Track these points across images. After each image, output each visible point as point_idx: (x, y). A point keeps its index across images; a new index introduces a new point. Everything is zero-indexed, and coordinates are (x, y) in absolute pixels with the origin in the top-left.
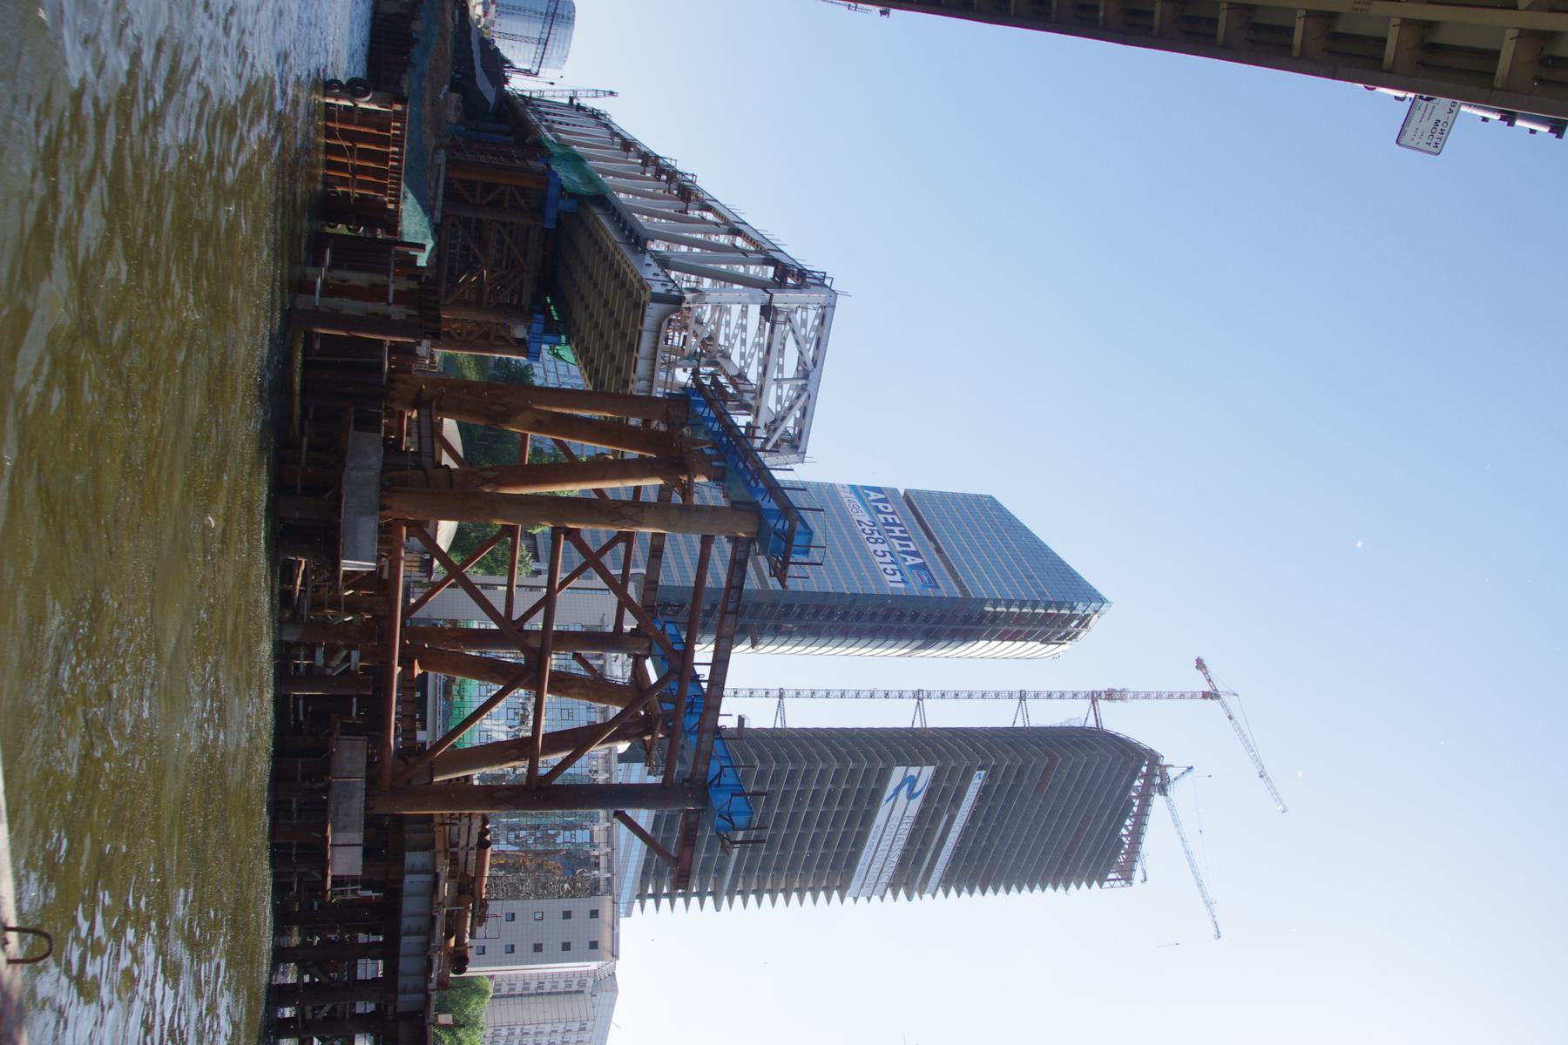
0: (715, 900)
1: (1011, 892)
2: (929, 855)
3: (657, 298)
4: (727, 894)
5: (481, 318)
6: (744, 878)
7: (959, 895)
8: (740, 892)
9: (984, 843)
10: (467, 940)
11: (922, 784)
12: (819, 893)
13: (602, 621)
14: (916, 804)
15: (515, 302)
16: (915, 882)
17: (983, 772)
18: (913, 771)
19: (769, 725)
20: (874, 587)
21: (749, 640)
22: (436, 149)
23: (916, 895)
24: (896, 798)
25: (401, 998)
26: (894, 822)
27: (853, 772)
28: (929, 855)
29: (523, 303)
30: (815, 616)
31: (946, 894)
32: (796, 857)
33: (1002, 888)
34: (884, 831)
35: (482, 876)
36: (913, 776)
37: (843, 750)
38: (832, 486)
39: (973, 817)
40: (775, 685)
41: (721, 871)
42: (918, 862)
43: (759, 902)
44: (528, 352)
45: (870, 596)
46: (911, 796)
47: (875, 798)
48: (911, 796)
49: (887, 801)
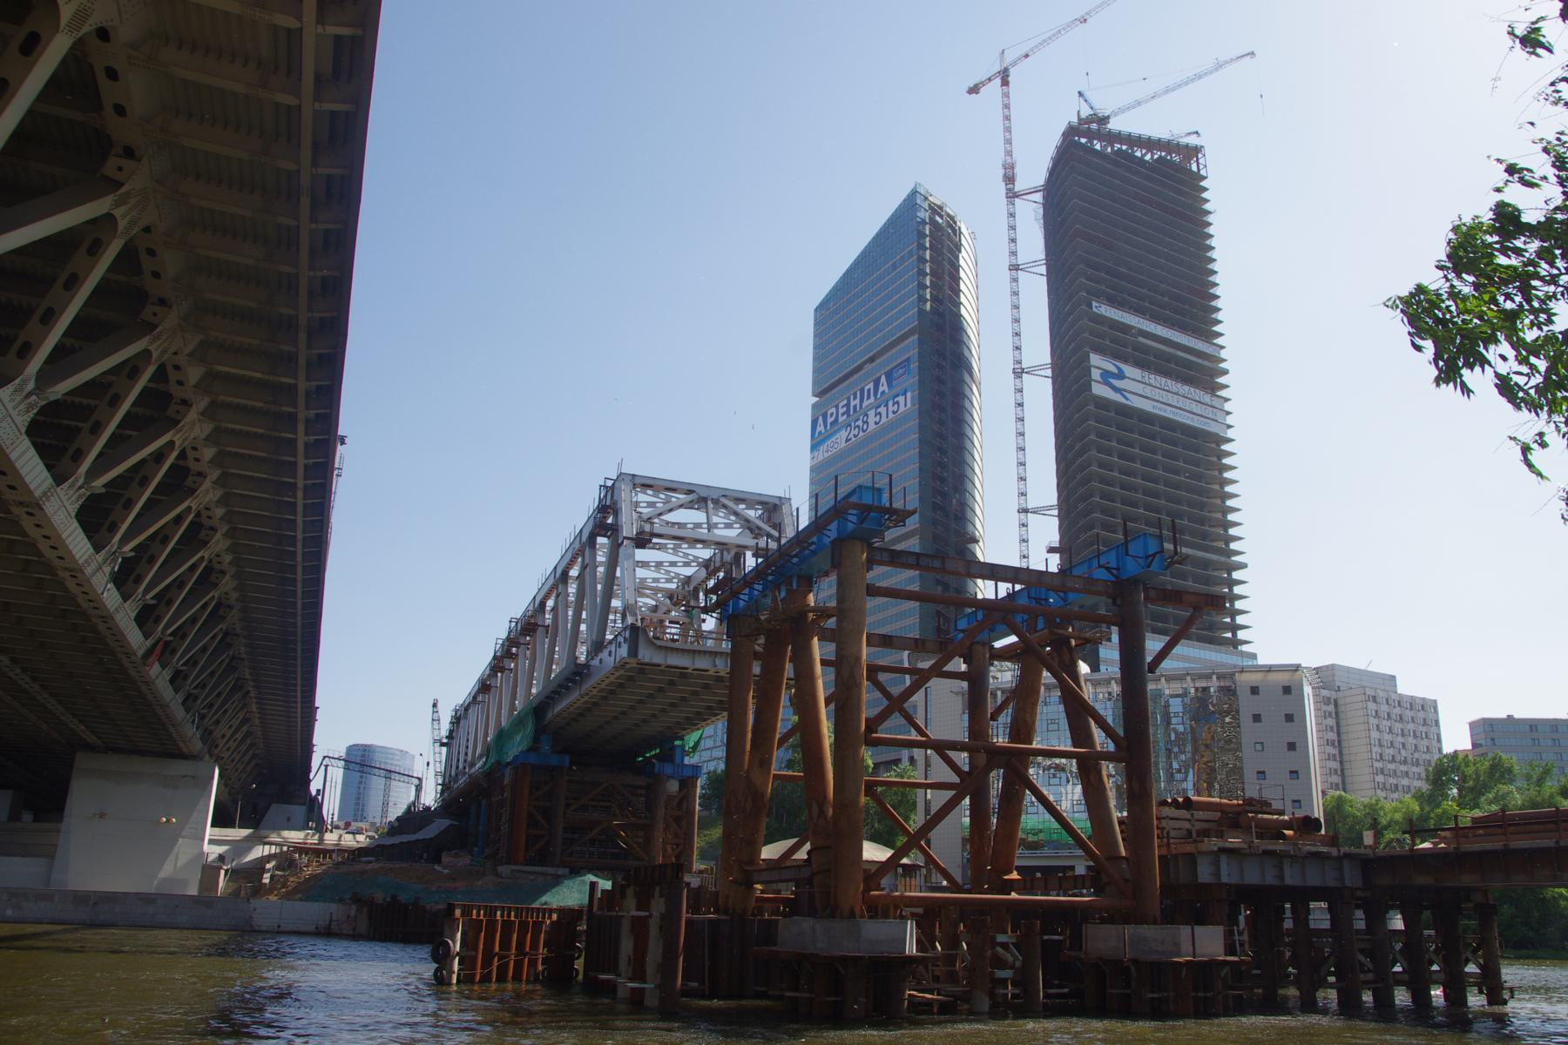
2: (1180, 354)
3: (633, 652)
5: (661, 825)
6: (1213, 541)
8: (1227, 544)
13: (957, 694)
14: (1129, 370)
17: (1094, 304)
18: (1096, 374)
19: (1056, 521)
21: (971, 546)
22: (498, 875)
23: (1222, 365)
24: (1124, 390)
25: (1348, 883)
26: (1148, 391)
27: (1101, 435)
28: (1180, 354)
29: (644, 784)
30: (943, 480)
38: (813, 469)
40: (1015, 518)
41: (1206, 564)
44: (692, 777)
46: (1121, 375)
47: (1125, 411)
49: (1127, 399)
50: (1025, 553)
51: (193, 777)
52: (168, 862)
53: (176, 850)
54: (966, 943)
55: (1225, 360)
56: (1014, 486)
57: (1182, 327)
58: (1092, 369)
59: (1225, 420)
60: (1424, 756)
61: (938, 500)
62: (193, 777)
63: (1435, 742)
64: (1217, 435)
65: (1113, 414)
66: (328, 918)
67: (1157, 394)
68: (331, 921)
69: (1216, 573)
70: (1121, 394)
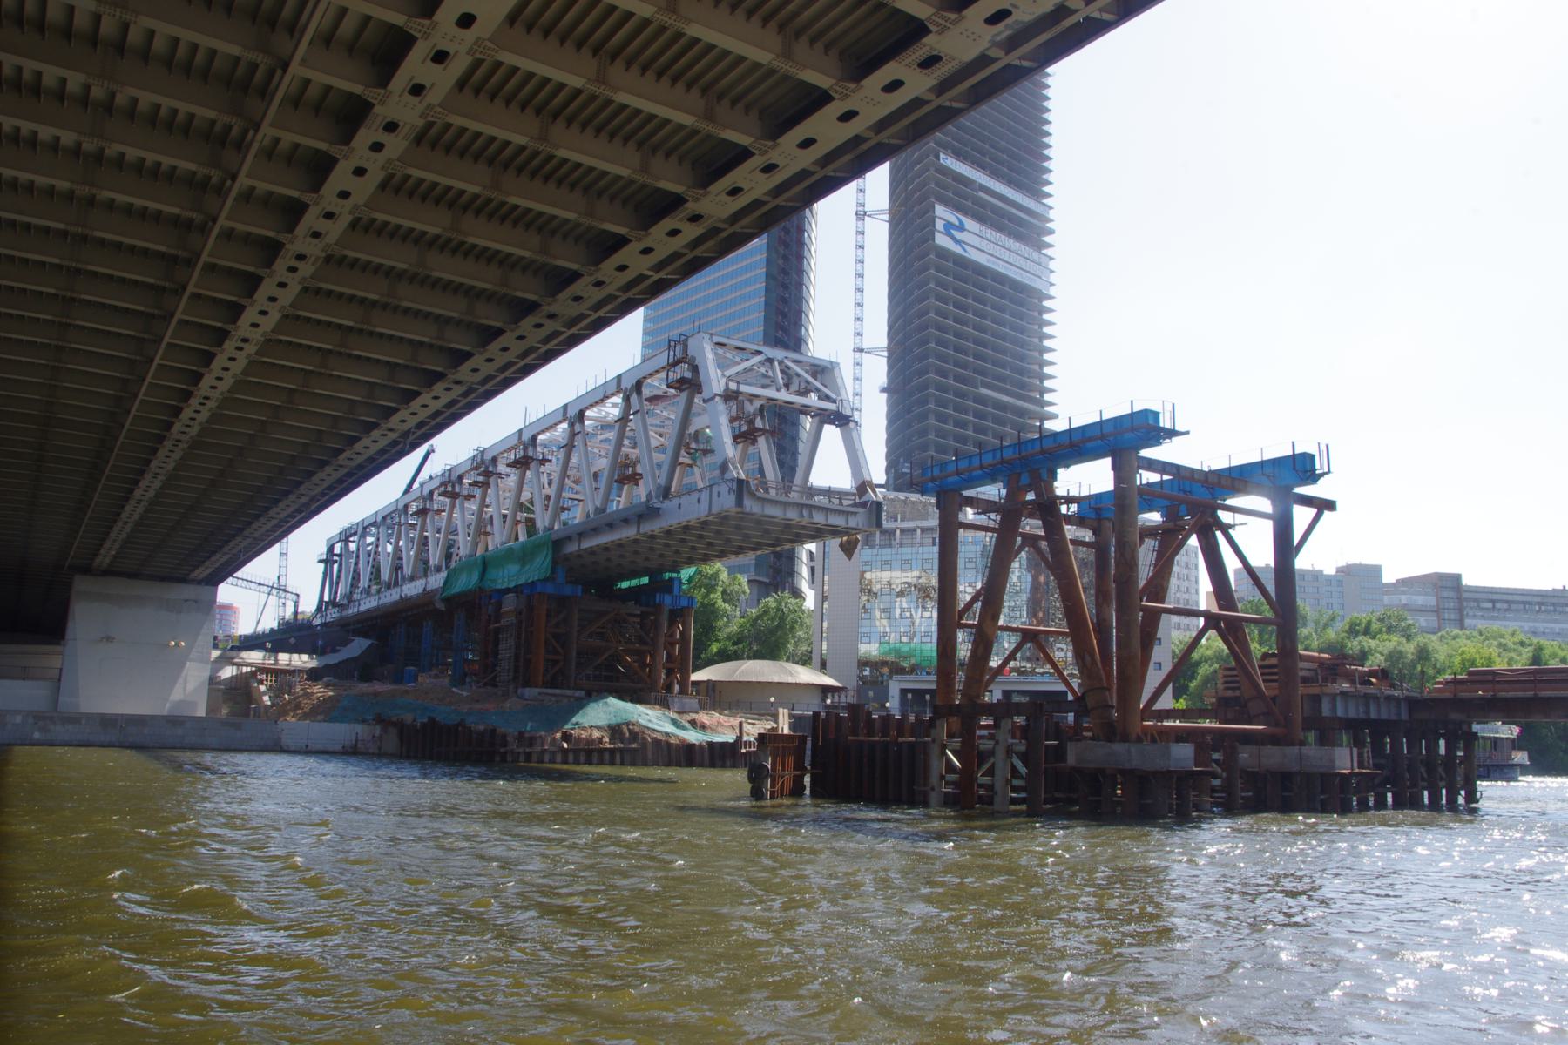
0: (1048, 419)
1: (1050, 131)
2: (1014, 211)
4: (1043, 407)
7: (1050, 183)
8: (1042, 395)
9: (1005, 156)
10: (1366, 669)
11: (952, 217)
14: (970, 224)
15: (639, 620)
17: (942, 156)
18: (939, 225)
22: (521, 697)
23: (1049, 225)
24: (964, 242)
26: (984, 245)
27: (939, 284)
28: (1014, 211)
29: (639, 612)
34: (992, 255)
35: (1319, 658)
39: (981, 166)
41: (1022, 413)
44: (688, 607)
46: (961, 228)
48: (961, 228)
49: (965, 251)
50: (858, 390)
51: (196, 602)
52: (177, 686)
53: (183, 675)
54: (950, 751)
55: (1051, 221)
56: (850, 326)
57: (1010, 182)
59: (1048, 277)
60: (1184, 596)
62: (196, 602)
63: (1193, 583)
66: (354, 738)
68: (357, 741)
69: (1029, 421)
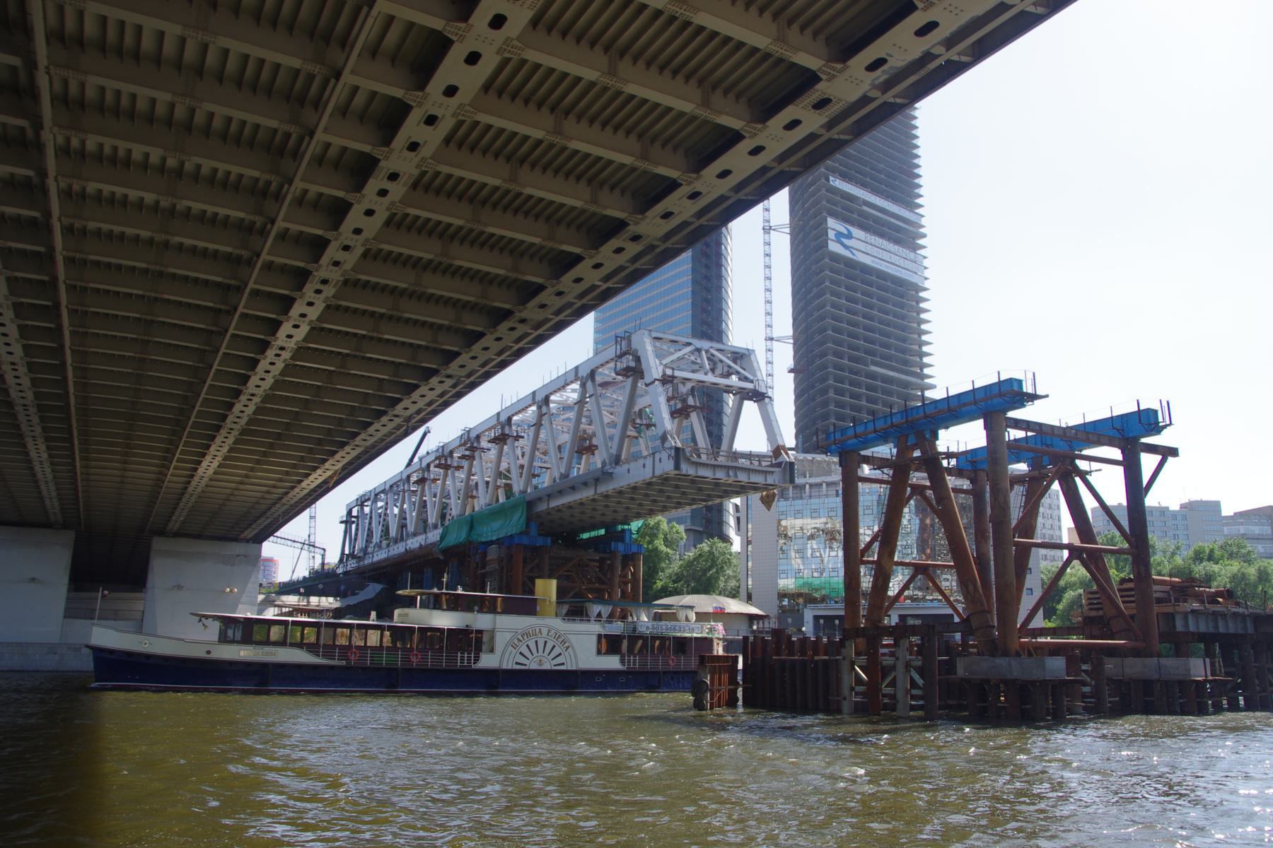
2: (892, 220)
4: (923, 380)
6: (911, 367)
7: (921, 196)
8: (922, 370)
11: (841, 228)
12: (921, 297)
14: (856, 232)
16: (912, 232)
17: (831, 178)
18: (831, 234)
19: (791, 347)
20: (685, 267)
23: (922, 230)
25: (1249, 632)
26: (869, 249)
28: (892, 220)
31: (920, 206)
32: (896, 326)
33: (917, 181)
36: (835, 235)
37: (815, 291)
39: (863, 185)
41: (906, 385)
42: (898, 229)
43: (928, 343)
45: (693, 270)
46: (849, 236)
47: (851, 264)
48: (849, 236)
51: (245, 556)
55: (923, 227)
57: (895, 200)
58: (829, 230)
61: (705, 328)
62: (245, 556)
63: (1056, 522)
64: (917, 284)
65: (842, 266)
67: (874, 251)
69: (913, 392)
70: (851, 251)
